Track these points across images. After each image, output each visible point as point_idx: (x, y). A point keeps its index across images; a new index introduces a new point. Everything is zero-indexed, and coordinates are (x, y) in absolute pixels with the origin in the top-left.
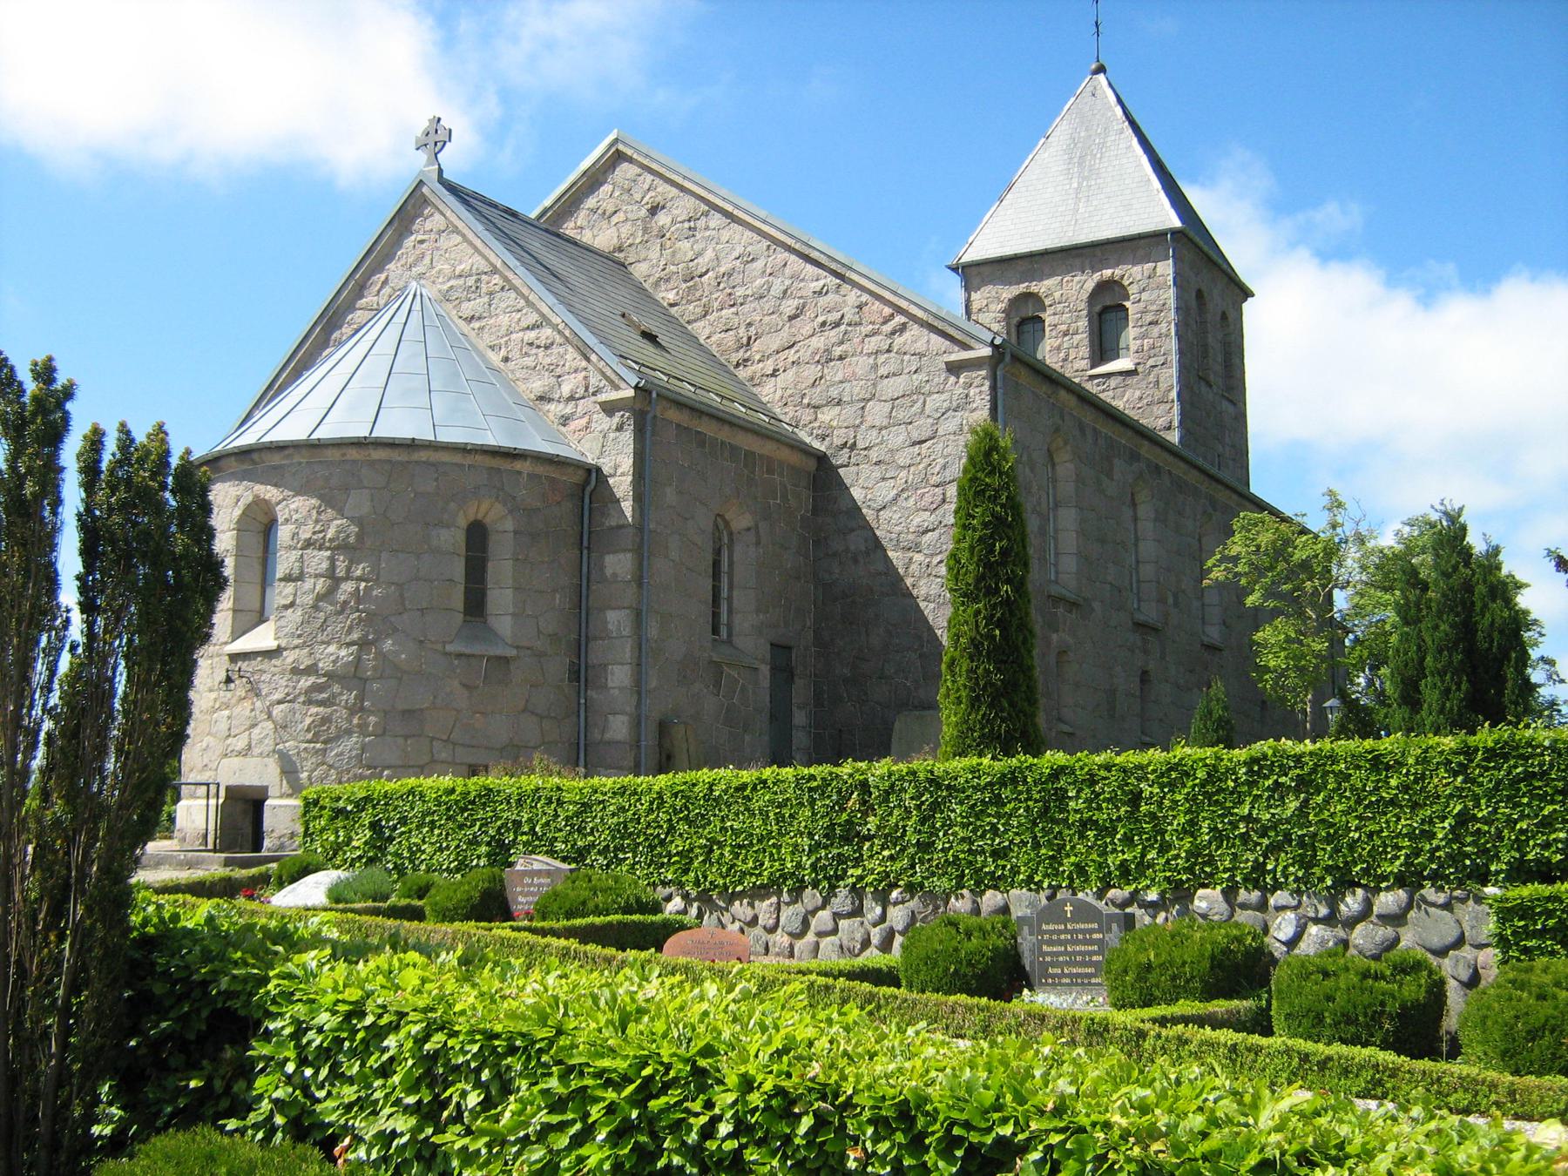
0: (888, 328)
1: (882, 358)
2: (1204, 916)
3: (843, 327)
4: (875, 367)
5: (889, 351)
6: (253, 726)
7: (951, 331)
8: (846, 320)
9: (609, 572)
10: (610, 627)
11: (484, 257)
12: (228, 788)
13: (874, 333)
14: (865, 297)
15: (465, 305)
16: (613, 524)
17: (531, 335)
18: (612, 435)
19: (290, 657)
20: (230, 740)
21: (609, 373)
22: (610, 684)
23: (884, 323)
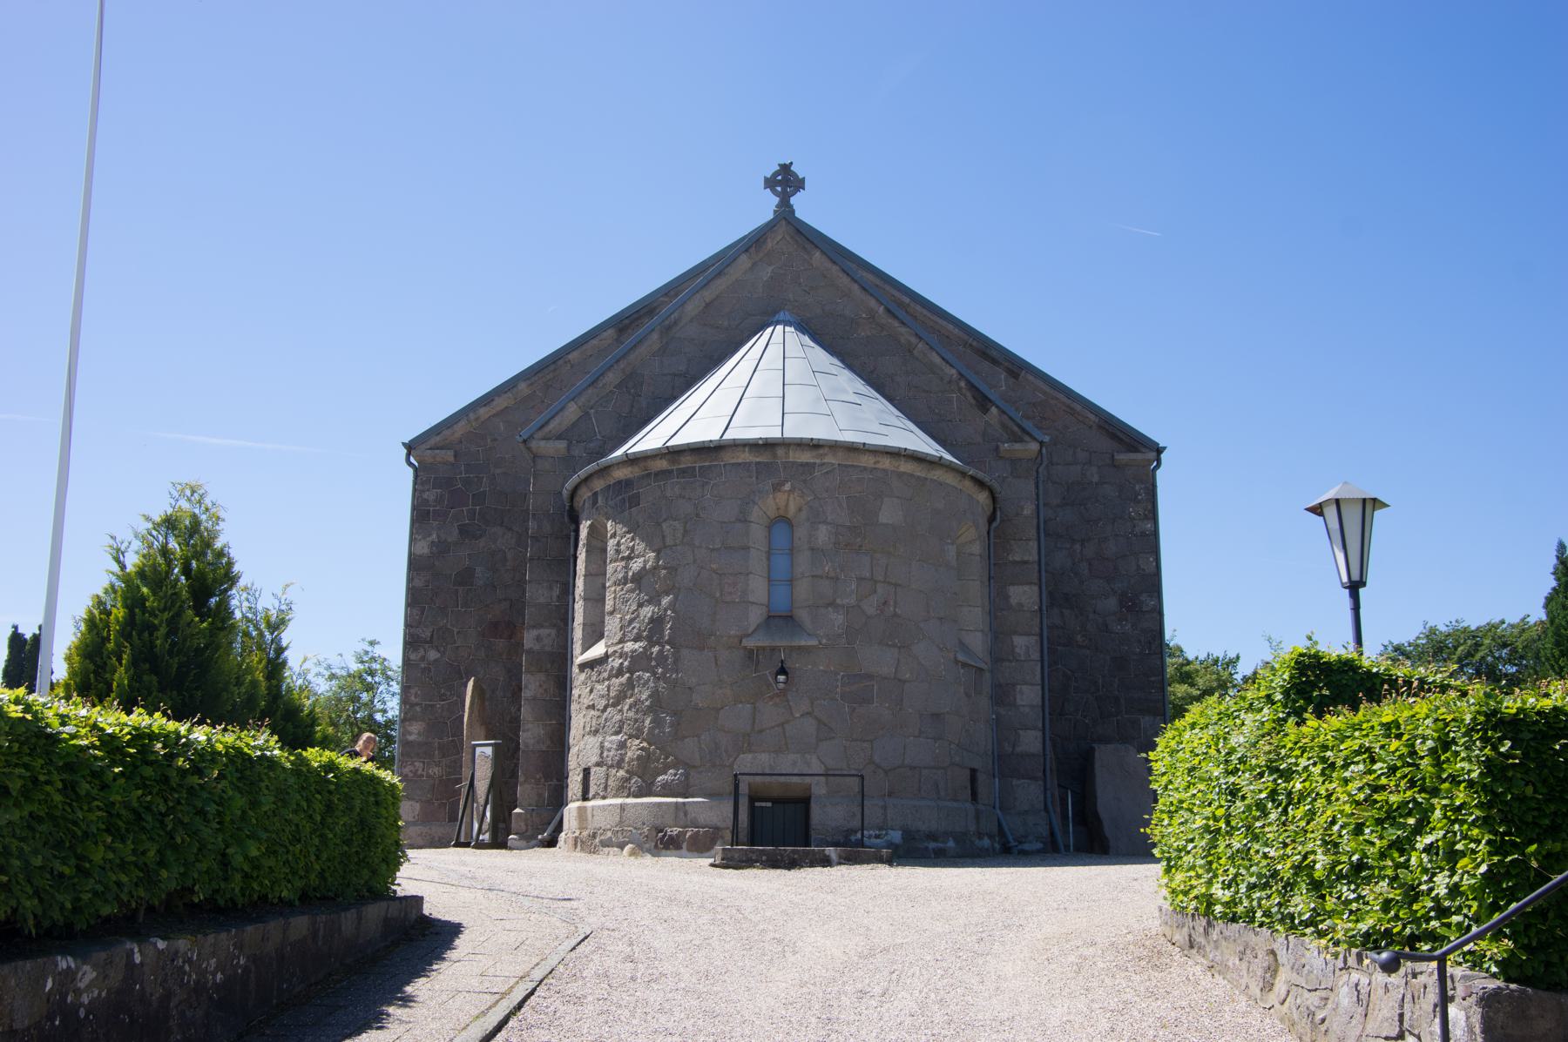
9: (1013, 601)
22: (1019, 702)
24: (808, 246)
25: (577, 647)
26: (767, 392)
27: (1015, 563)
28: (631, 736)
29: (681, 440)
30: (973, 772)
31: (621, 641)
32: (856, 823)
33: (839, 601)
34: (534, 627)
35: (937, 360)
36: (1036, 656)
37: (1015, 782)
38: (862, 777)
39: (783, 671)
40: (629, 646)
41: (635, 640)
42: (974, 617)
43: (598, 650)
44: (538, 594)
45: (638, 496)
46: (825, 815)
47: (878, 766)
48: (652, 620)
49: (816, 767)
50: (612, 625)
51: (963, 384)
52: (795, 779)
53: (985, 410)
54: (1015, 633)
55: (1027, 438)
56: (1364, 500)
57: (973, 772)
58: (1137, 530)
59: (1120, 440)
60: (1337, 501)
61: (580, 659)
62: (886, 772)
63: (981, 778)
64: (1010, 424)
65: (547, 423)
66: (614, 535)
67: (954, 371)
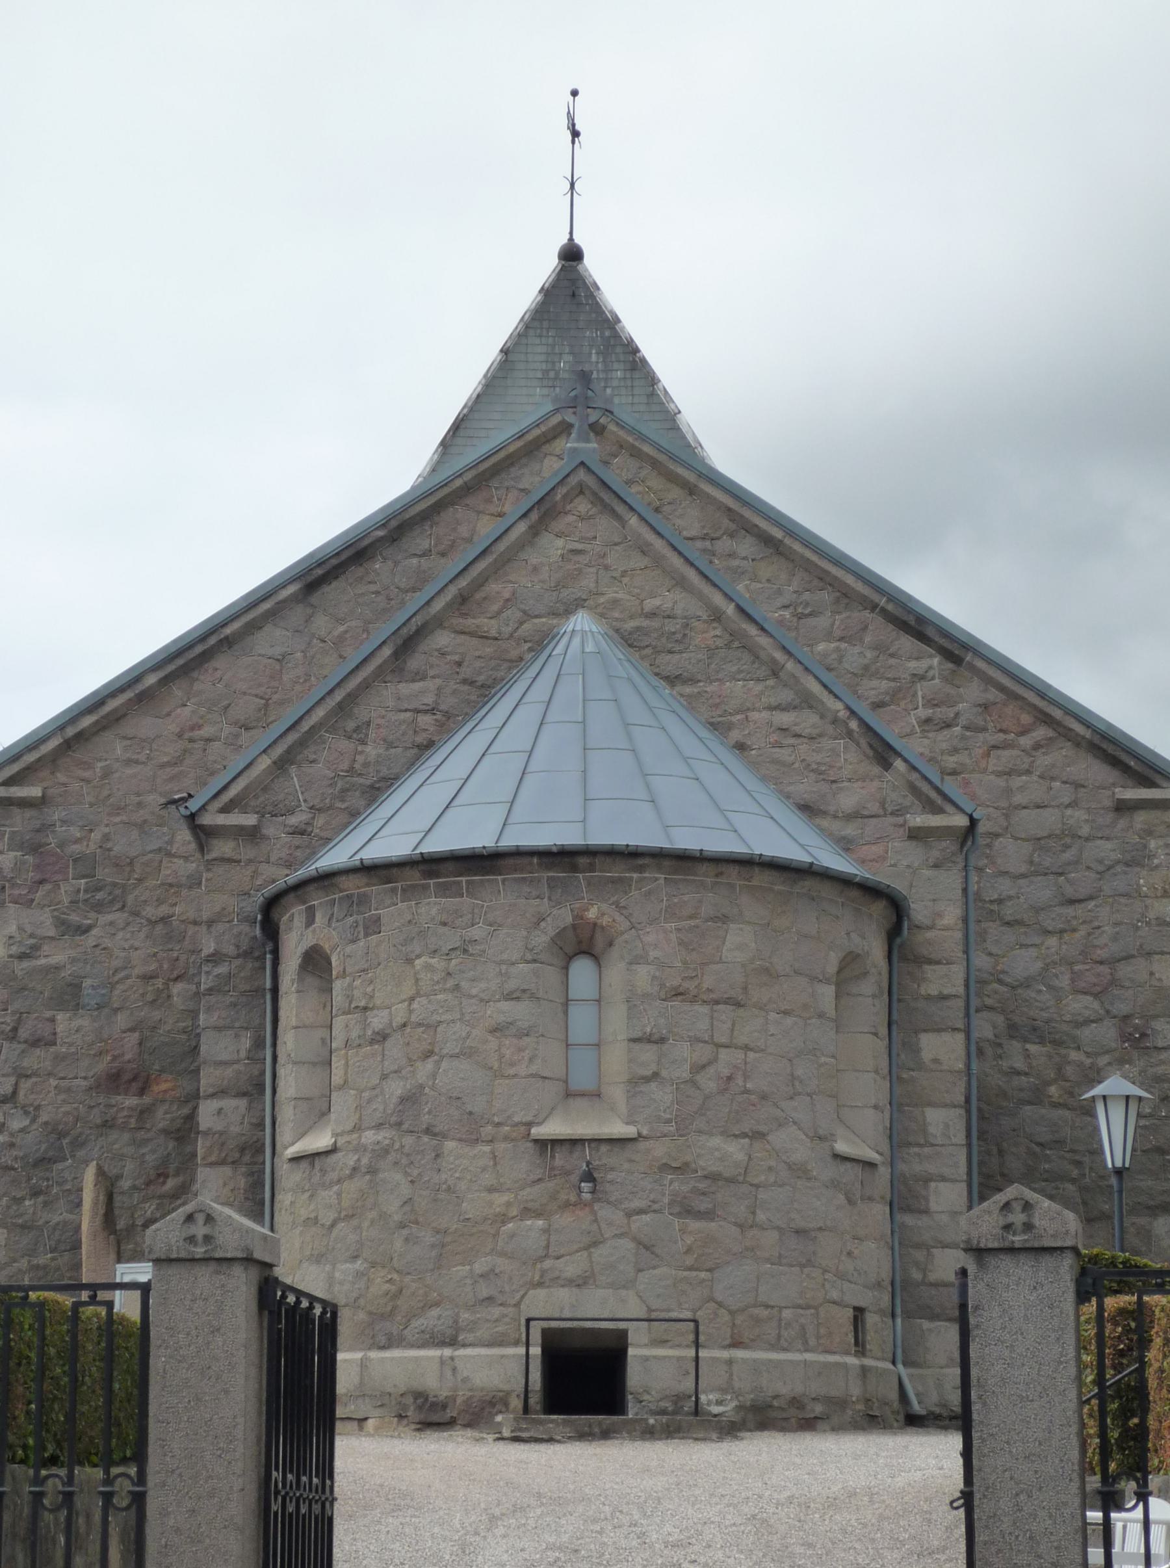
0: (1026, 741)
1: (1017, 781)
2: (346, 1395)
3: (957, 730)
4: (1008, 791)
5: (1028, 772)
6: (595, 1244)
7: (1124, 757)
8: (962, 721)
9: (926, 1055)
10: (932, 1129)
11: (701, 597)
12: (545, 1333)
13: (1006, 746)
14: (993, 695)
15: (665, 658)
16: (933, 990)
17: (785, 719)
18: (927, 873)
19: (659, 1150)
20: (548, 1264)
21: (925, 788)
22: (933, 1206)
23: (1022, 734)
24: (620, 509)
25: (285, 1133)
26: (557, 753)
27: (928, 998)
28: (373, 1265)
29: (436, 845)
30: (859, 1311)
31: (357, 1128)
32: (688, 1385)
33: (664, 1073)
34: (212, 1096)
35: (815, 687)
36: (961, 1138)
37: (926, 1324)
38: (582, 463)
39: (589, 1177)
40: (369, 1137)
41: (379, 1126)
42: (867, 1088)
43: (320, 1141)
44: (222, 1050)
45: (378, 920)
46: (650, 1367)
47: (720, 1304)
48: (403, 1100)
49: (634, 1308)
50: (343, 1104)
51: (854, 725)
52: (588, 1324)
53: (886, 765)
54: (931, 1104)
55: (949, 808)
56: (1128, 1097)
57: (859, 1311)
58: (1151, 915)
59: (1125, 769)
60: (1104, 1097)
61: (291, 1151)
62: (732, 1313)
63: (871, 1319)
64: (925, 788)
65: (225, 788)
66: (343, 975)
67: (839, 706)
